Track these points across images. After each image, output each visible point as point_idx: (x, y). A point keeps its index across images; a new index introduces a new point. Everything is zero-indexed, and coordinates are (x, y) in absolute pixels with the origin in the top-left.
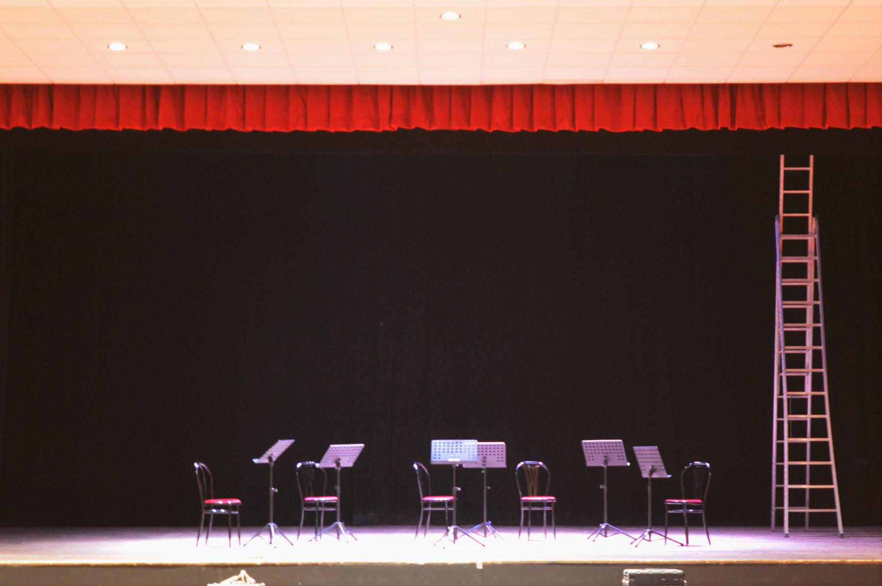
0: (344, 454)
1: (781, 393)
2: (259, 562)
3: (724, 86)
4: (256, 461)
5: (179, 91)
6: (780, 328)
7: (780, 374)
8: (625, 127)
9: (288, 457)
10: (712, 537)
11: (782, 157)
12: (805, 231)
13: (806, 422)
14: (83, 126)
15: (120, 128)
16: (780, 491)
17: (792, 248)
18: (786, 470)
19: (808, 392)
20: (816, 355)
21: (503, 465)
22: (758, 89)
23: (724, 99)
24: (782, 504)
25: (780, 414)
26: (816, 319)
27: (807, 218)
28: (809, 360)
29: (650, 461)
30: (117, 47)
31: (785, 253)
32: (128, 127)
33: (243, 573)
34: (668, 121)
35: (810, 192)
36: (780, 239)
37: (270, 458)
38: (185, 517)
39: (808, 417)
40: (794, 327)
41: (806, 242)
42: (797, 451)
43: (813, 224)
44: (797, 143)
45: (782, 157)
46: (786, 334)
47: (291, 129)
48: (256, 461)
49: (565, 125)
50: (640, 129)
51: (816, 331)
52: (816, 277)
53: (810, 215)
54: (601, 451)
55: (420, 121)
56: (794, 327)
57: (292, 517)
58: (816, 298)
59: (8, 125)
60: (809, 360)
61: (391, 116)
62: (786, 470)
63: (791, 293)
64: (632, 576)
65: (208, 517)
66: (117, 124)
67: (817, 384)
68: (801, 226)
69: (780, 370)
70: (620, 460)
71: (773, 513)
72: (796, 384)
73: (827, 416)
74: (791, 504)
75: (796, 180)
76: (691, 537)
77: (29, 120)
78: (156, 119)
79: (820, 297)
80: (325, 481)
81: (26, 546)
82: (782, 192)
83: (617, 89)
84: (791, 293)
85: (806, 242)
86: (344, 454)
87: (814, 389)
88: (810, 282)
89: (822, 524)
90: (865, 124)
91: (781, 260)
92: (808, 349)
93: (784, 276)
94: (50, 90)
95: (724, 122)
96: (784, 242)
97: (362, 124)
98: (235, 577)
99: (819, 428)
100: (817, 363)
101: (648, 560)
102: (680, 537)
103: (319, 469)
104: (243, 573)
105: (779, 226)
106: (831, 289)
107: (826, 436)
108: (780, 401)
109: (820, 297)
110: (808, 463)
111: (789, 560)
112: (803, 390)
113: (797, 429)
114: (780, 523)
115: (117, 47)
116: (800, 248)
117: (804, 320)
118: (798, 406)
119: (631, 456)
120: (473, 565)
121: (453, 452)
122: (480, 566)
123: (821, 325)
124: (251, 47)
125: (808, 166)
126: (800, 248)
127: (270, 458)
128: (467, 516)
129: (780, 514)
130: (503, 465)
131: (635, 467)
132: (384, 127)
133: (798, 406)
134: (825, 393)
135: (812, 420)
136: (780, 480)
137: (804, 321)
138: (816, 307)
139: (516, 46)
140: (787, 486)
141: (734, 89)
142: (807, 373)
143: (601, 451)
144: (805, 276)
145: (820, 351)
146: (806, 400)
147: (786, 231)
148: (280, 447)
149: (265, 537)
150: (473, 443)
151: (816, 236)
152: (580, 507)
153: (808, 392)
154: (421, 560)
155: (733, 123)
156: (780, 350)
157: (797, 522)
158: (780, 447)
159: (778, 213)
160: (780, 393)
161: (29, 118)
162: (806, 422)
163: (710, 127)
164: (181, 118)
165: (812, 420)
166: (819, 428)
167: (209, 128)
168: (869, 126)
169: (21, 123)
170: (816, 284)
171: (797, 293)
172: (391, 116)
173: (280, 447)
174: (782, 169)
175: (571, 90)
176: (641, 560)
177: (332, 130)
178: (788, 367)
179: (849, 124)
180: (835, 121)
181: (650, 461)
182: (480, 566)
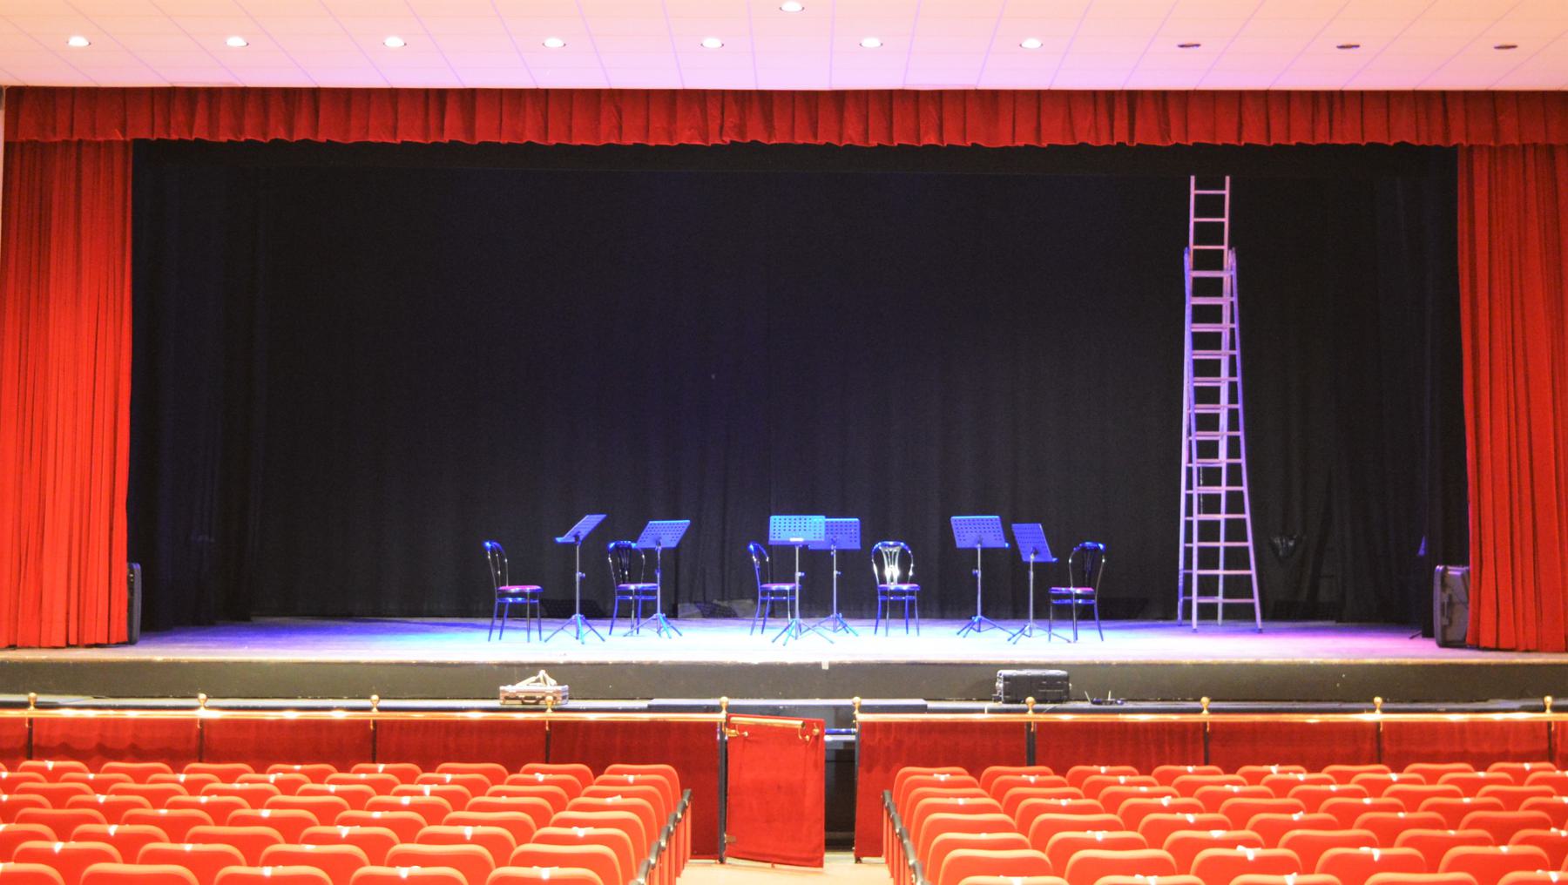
0: (666, 533)
1: (1190, 461)
2: (561, 660)
3: (1121, 92)
4: (559, 540)
5: (469, 98)
6: (1189, 383)
7: (1189, 438)
8: (1004, 141)
9: (599, 532)
10: (1105, 633)
11: (1193, 178)
12: (1220, 267)
13: (1219, 496)
14: (353, 138)
15: (399, 141)
16: (1188, 577)
17: (1202, 287)
18: (1195, 553)
19: (1222, 460)
20: (1233, 414)
21: (856, 546)
22: (1162, 97)
23: (1121, 111)
24: (1190, 594)
25: (1189, 512)
26: (1232, 373)
27: (1222, 251)
28: (1223, 421)
29: (1034, 545)
30: (394, 42)
31: (1196, 293)
32: (407, 139)
33: (542, 673)
34: (1054, 135)
35: (1226, 220)
36: (1191, 274)
37: (576, 537)
38: (472, 604)
39: (1222, 490)
40: (1206, 382)
41: (1221, 280)
42: (1208, 531)
43: (1229, 259)
44: (1209, 161)
45: (1193, 178)
46: (1197, 389)
47: (604, 142)
48: (559, 540)
49: (930, 139)
50: (1020, 143)
51: (1232, 386)
52: (1232, 321)
53: (1225, 247)
54: (975, 531)
55: (756, 133)
56: (1206, 382)
57: (600, 608)
58: (1232, 347)
59: (670, 138)
60: (1223, 421)
61: (722, 127)
62: (1195, 553)
63: (1203, 368)
64: (1006, 679)
65: (502, 605)
66: (395, 137)
67: (1233, 451)
68: (1215, 261)
69: (1189, 433)
70: (996, 540)
71: (1181, 577)
72: (1208, 449)
73: (1247, 516)
74: (1200, 594)
75: (1209, 206)
76: (1080, 633)
77: (290, 130)
78: (441, 130)
79: (1239, 371)
80: (639, 566)
81: (270, 650)
82: (1193, 220)
83: (995, 95)
84: (1203, 368)
85: (1221, 280)
86: (666, 533)
87: (1230, 456)
88: (1225, 327)
89: (1238, 616)
90: (1289, 138)
91: (1192, 301)
92: (1223, 409)
93: (1195, 320)
94: (315, 95)
95: (1121, 136)
96: (1195, 279)
97: (687, 136)
98: (533, 679)
99: (1236, 558)
100: (1233, 425)
101: (1027, 660)
102: (1068, 633)
103: (636, 550)
104: (542, 673)
105: (1188, 260)
106: (1253, 390)
107: (1243, 512)
108: (1189, 470)
109: (1239, 371)
110: (1221, 572)
111: (1194, 661)
112: (1216, 456)
113: (1208, 531)
114: (1187, 615)
115: (394, 42)
116: (1214, 287)
117: (1217, 401)
118: (1210, 504)
119: (1010, 537)
120: (818, 665)
121: (796, 530)
122: (825, 667)
123: (1239, 406)
124: (554, 43)
125: (1223, 216)
126: (1214, 287)
127: (576, 537)
128: (815, 604)
129: (1188, 605)
130: (856, 546)
131: (1014, 551)
132: (714, 140)
133: (1211, 476)
134: (1244, 489)
135: (1227, 521)
136: (1188, 564)
137: (1218, 375)
138: (1232, 358)
139: (871, 42)
140: (1196, 572)
141: (1132, 97)
142: (1222, 436)
143: (975, 531)
144: (1220, 321)
145: (1238, 438)
146: (1220, 469)
147: (1196, 267)
148: (587, 524)
149: (572, 630)
150: (819, 520)
151: (1234, 273)
152: (945, 593)
153: (1222, 460)
154: (755, 659)
155: (1132, 140)
156: (1189, 409)
157: (1207, 613)
158: (1188, 551)
159: (1187, 244)
160: (1189, 461)
161: (290, 130)
162: (1219, 496)
163: (1104, 142)
164: (470, 129)
165: (1226, 549)
166: (1235, 530)
167: (504, 141)
168: (1293, 143)
169: (281, 135)
170: (1232, 331)
171: (1212, 341)
172: (722, 127)
173: (587, 524)
174: (1193, 192)
175: (939, 98)
176: (1017, 660)
177: (652, 144)
178: (1199, 457)
179: (1269, 137)
180: (1253, 136)
181: (1034, 545)
182: (825, 667)
